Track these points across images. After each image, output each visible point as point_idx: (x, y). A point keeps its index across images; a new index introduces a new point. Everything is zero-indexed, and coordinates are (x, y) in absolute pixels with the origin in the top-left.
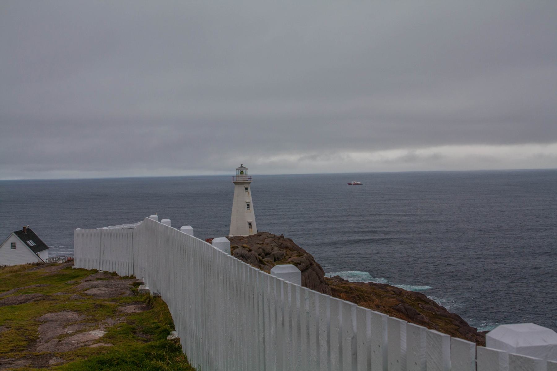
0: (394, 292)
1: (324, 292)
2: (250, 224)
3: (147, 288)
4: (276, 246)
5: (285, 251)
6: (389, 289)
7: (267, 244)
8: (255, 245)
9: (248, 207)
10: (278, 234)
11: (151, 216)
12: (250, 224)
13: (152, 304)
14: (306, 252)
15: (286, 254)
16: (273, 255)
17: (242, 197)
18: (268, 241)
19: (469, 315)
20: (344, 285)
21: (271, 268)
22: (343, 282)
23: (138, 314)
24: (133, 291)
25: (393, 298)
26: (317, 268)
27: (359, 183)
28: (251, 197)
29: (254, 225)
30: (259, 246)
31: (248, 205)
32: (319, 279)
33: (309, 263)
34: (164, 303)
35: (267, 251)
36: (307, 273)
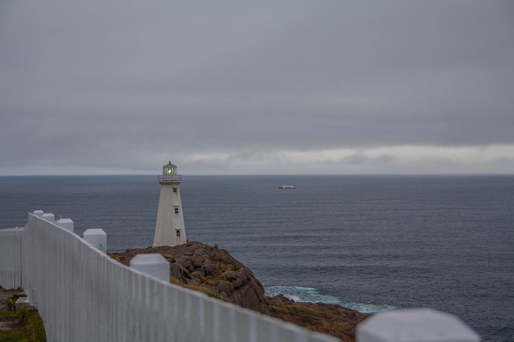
0: (346, 314)
1: (263, 313)
2: (178, 232)
3: (27, 301)
4: (208, 257)
5: (218, 263)
6: (341, 310)
7: (197, 256)
8: (183, 256)
9: (176, 212)
10: (211, 244)
11: (36, 212)
12: (178, 232)
13: (27, 320)
14: (243, 266)
15: (220, 268)
16: (204, 268)
17: (170, 200)
18: (198, 252)
20: (288, 306)
21: (131, 259)
22: (288, 302)
23: (5, 332)
24: (10, 305)
25: (346, 321)
26: (256, 284)
27: (292, 187)
28: (180, 200)
29: (183, 233)
30: (187, 257)
31: (176, 209)
32: (258, 297)
33: (246, 278)
34: (39, 318)
35: (196, 264)
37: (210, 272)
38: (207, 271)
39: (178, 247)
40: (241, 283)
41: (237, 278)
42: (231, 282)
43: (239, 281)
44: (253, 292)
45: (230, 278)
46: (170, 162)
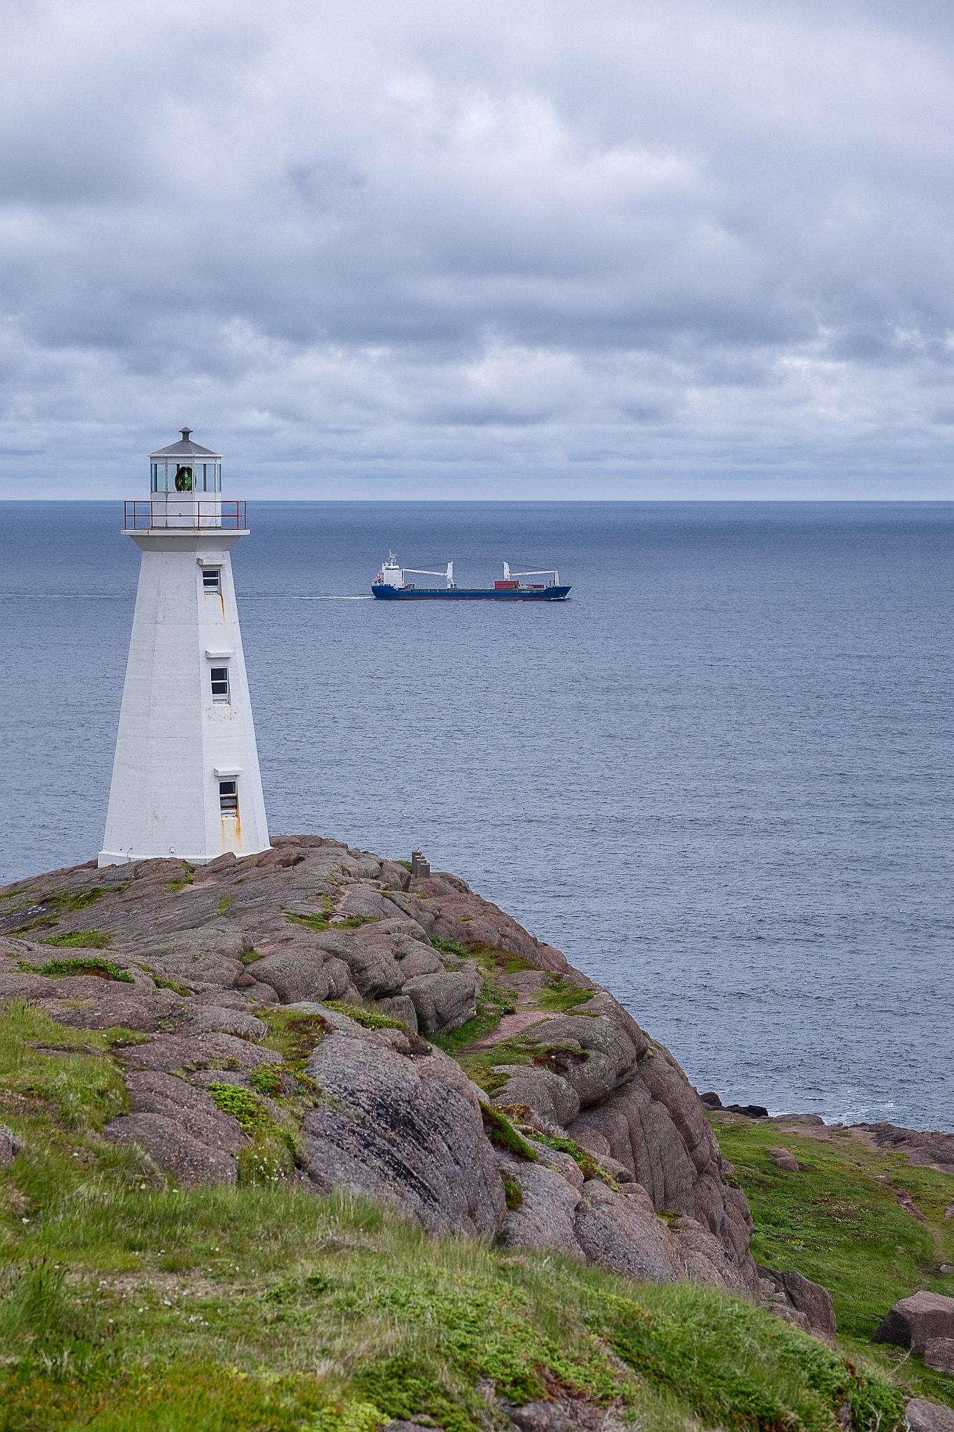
2: (227, 787)
9: (219, 689)
10: (397, 853)
12: (227, 787)
16: (415, 996)
19: (80, 716)
29: (251, 792)
31: (219, 674)
32: (691, 1145)
35: (375, 975)
36: (622, 1120)
37: (441, 1020)
38: (429, 1011)
39: (225, 867)
40: (613, 1074)
41: (592, 1053)
42: (560, 1069)
43: (599, 1067)
44: (670, 1125)
45: (550, 1052)
46: (186, 433)
